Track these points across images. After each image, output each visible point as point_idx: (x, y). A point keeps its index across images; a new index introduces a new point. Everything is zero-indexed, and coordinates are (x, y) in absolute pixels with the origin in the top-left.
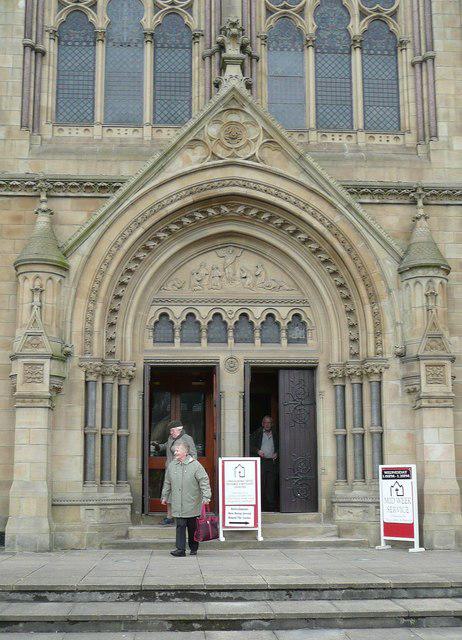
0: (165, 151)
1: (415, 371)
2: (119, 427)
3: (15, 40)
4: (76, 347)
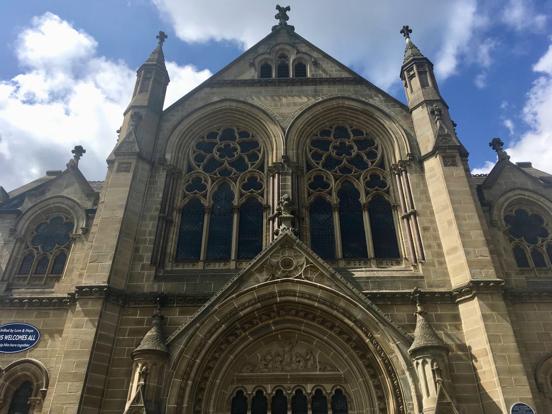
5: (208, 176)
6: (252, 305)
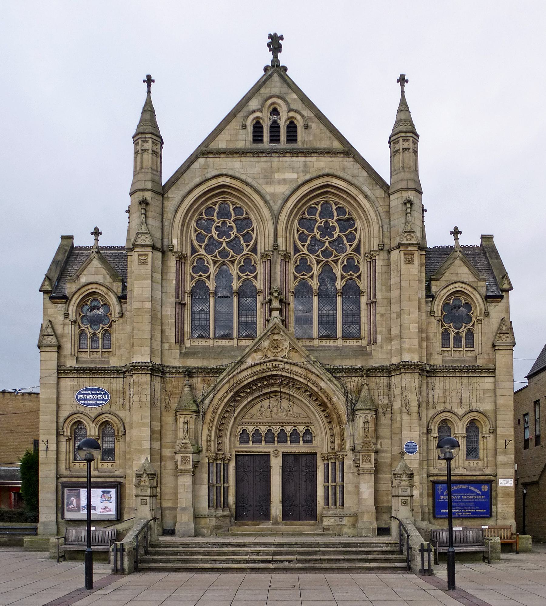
0: (243, 356)
2: (224, 483)
3: (171, 300)
4: (204, 446)
5: (210, 259)
6: (251, 377)
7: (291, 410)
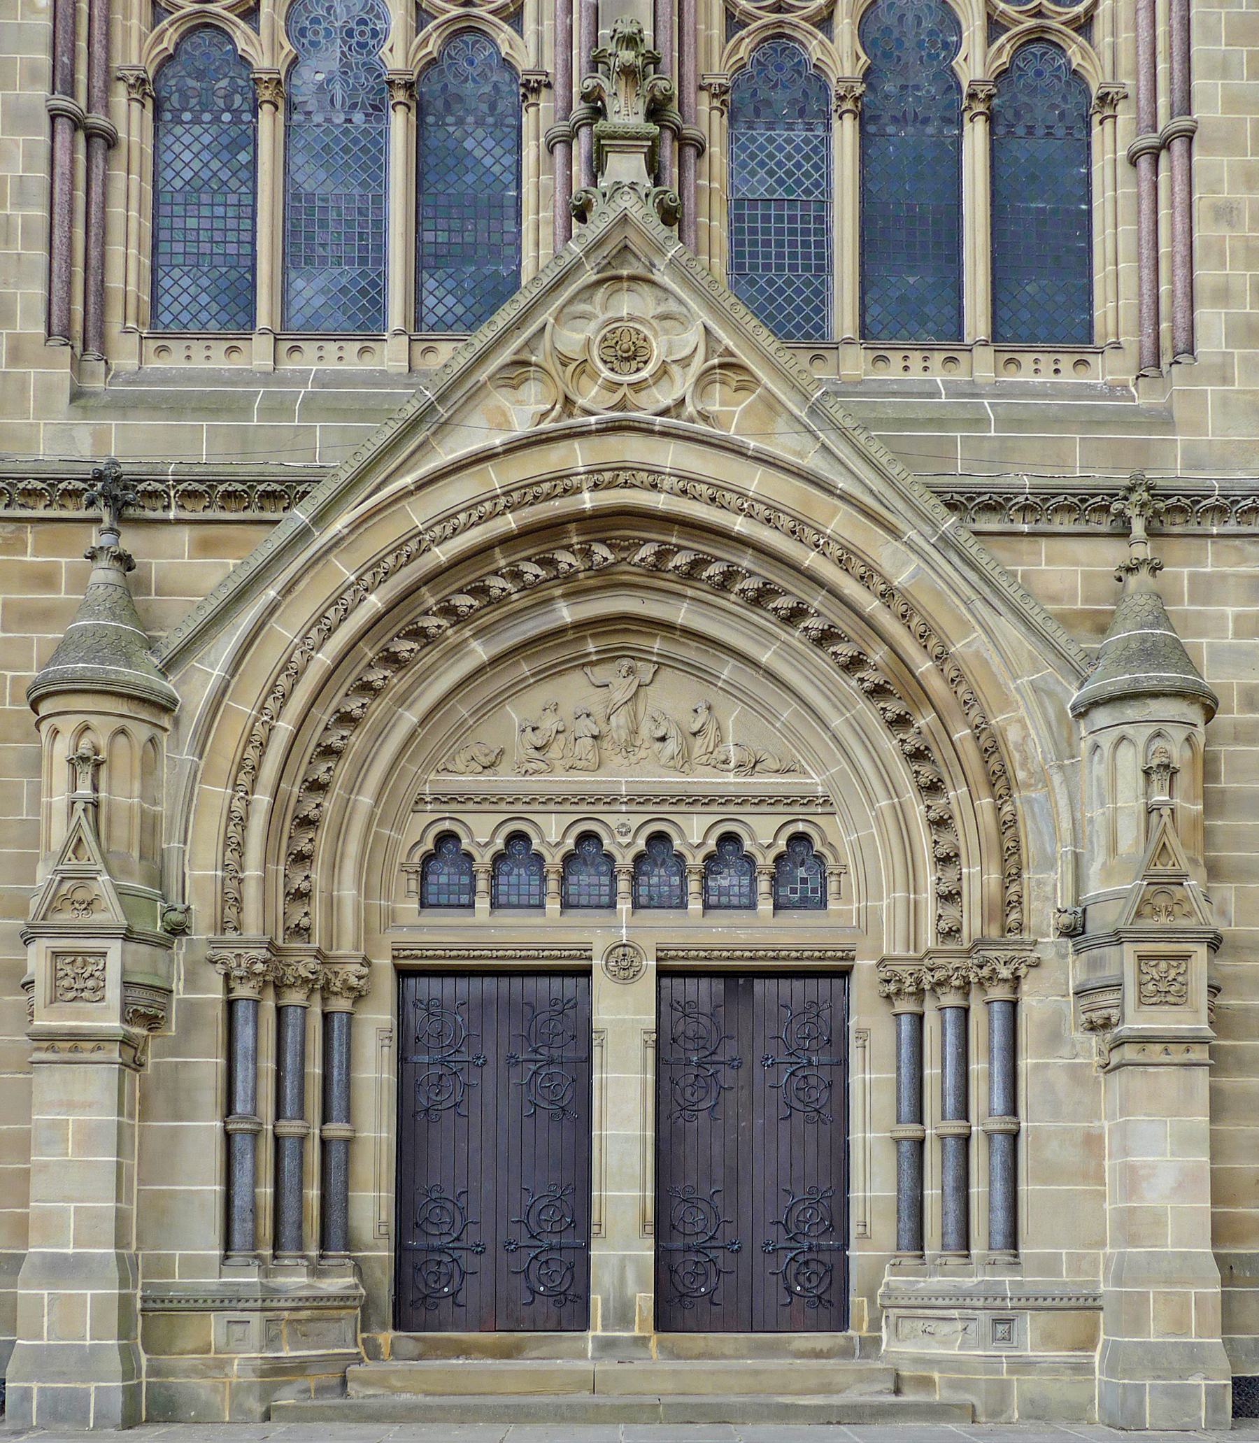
1: (1108, 974)
2: (325, 1119)
7: (711, 729)
